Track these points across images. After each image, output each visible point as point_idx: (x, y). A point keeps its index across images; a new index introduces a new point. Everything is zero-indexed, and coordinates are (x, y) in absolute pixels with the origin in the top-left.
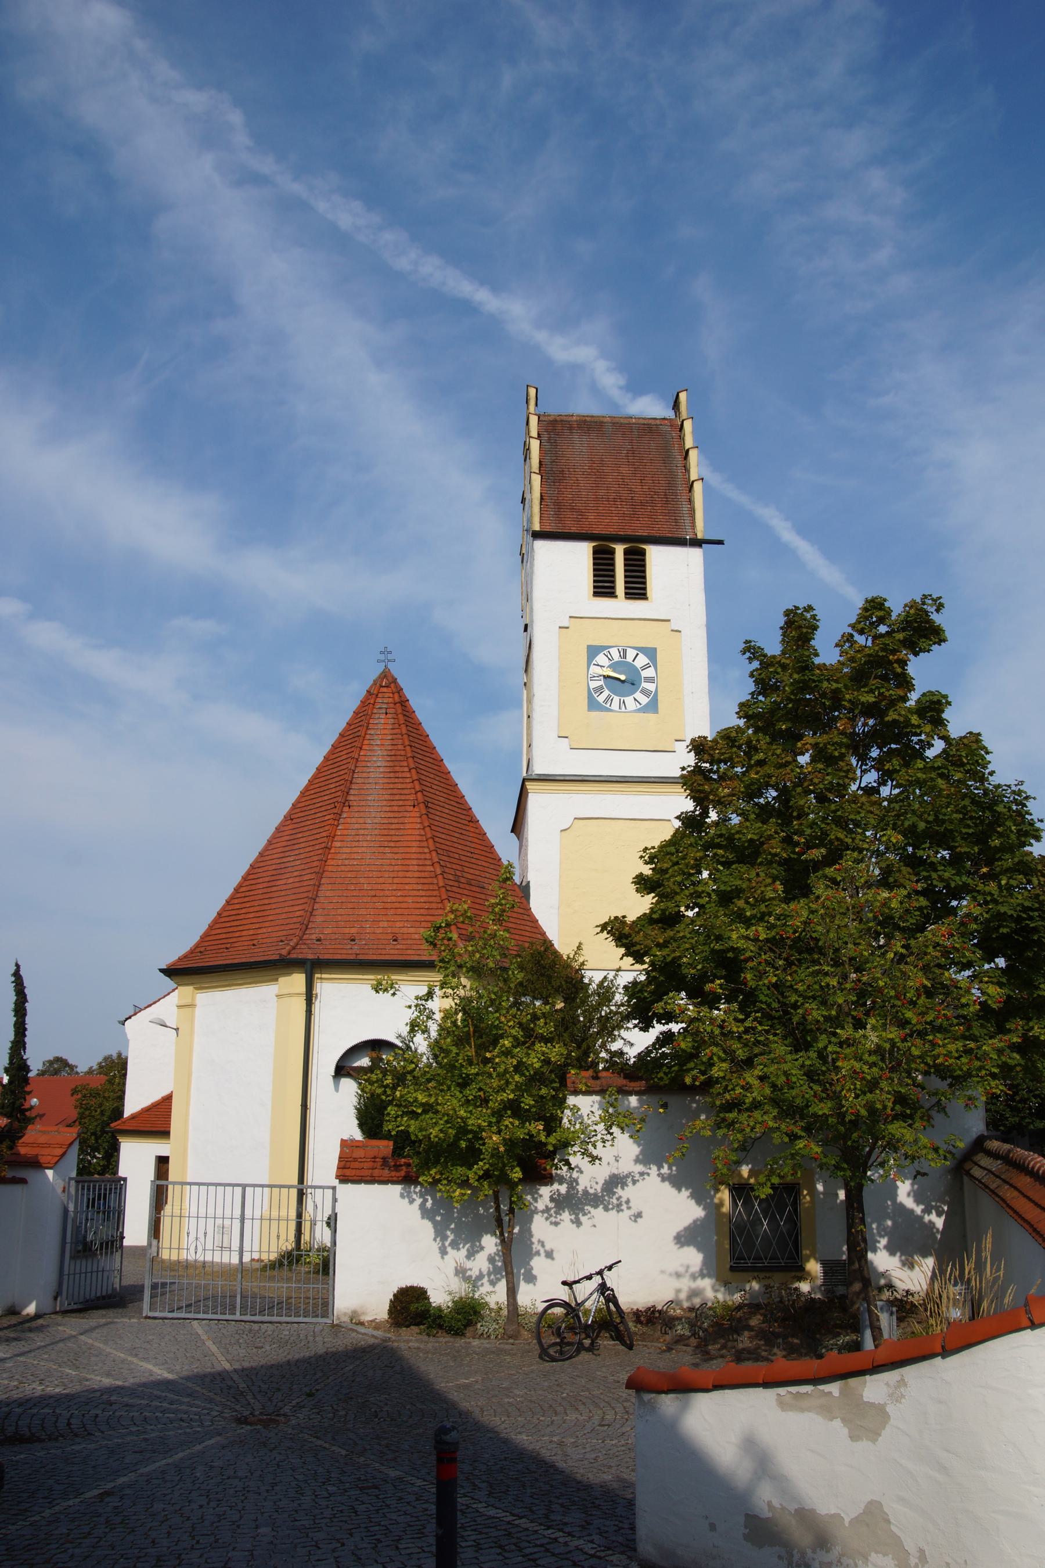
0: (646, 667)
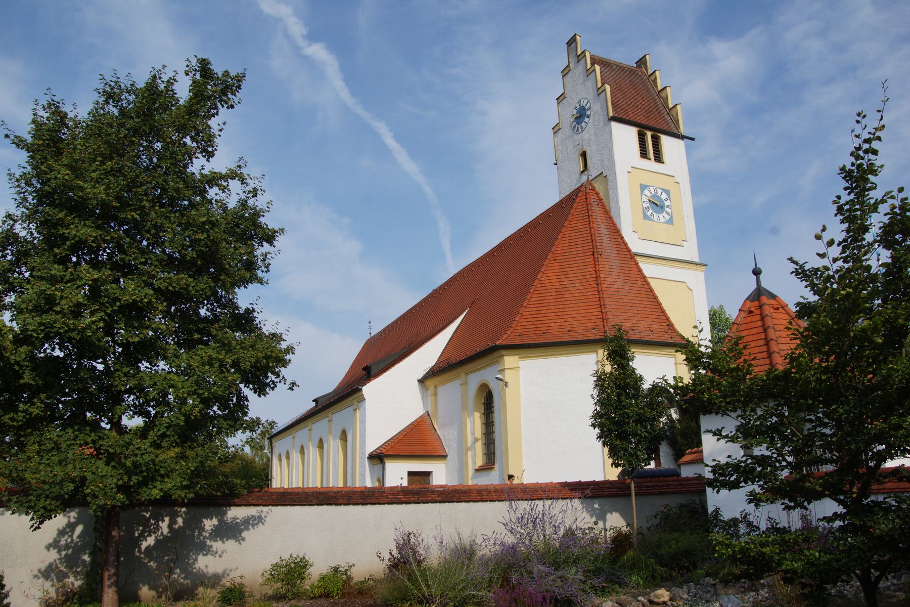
0: (666, 200)
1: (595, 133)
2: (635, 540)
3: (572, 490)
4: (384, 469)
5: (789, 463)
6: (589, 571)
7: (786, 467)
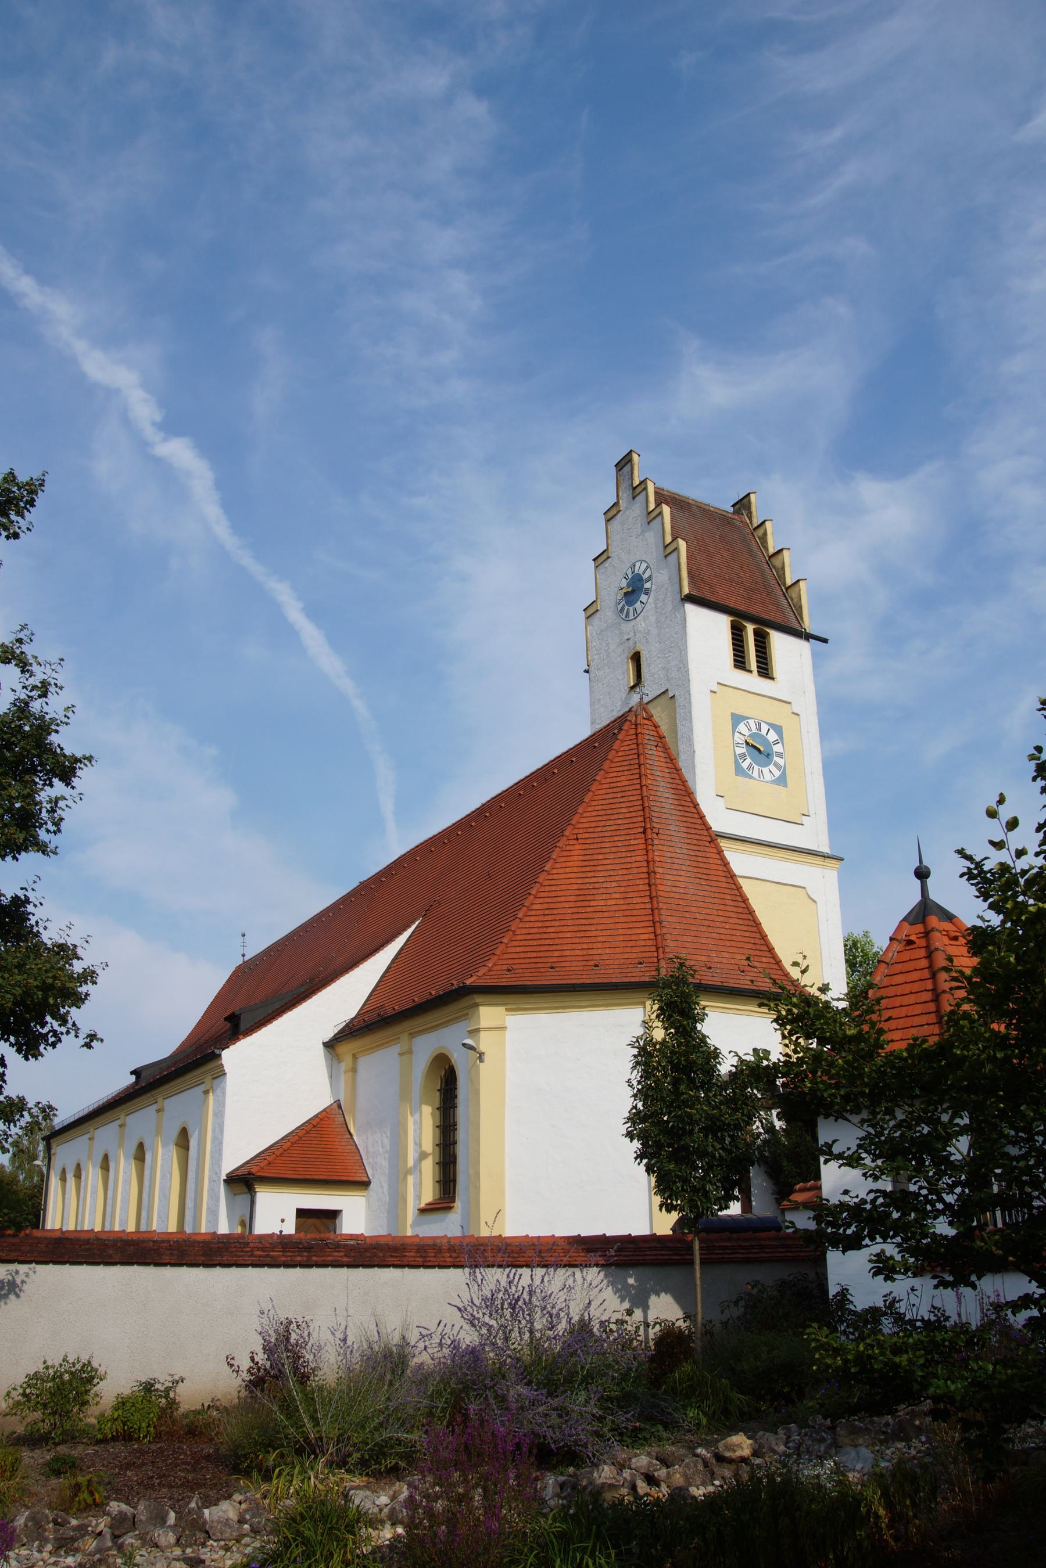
0: (776, 743)
1: (657, 621)
2: (697, 1345)
3: (589, 1251)
4: (253, 1203)
5: (948, 1206)
6: (610, 1399)
7: (942, 1212)
